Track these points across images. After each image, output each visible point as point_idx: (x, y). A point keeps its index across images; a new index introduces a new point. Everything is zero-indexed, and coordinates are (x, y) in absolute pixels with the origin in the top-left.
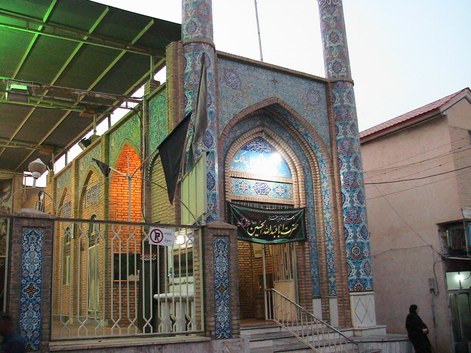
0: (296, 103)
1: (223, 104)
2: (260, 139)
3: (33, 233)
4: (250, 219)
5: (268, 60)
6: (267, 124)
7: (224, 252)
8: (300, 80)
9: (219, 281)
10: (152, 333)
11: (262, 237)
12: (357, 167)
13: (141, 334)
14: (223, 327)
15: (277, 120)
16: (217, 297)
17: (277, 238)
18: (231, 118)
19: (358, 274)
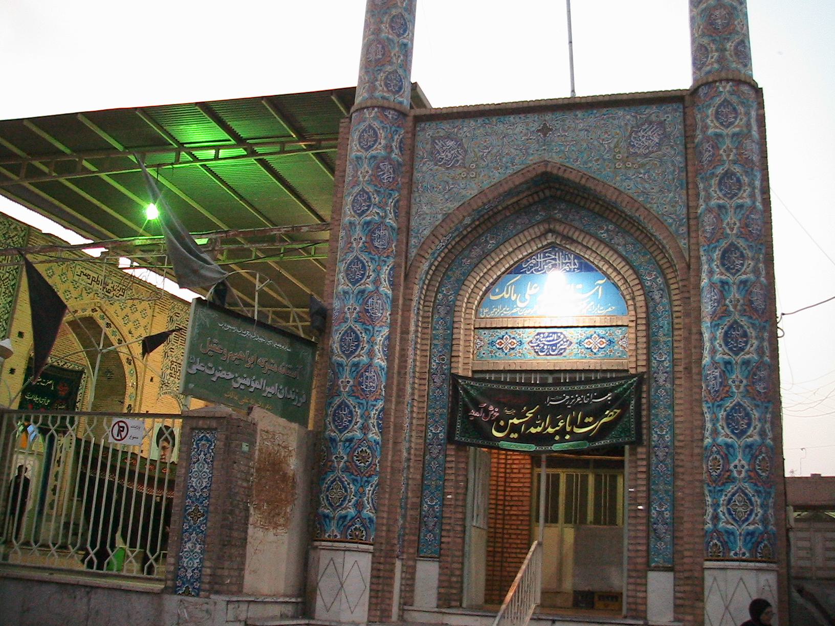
1: (424, 200)
2: (552, 246)
6: (559, 216)
7: (208, 455)
8: (613, 111)
9: (193, 502)
10: (94, 570)
12: (728, 269)
13: (141, 575)
14: (189, 575)
16: (186, 527)
17: (562, 440)
18: (437, 223)
19: (716, 518)
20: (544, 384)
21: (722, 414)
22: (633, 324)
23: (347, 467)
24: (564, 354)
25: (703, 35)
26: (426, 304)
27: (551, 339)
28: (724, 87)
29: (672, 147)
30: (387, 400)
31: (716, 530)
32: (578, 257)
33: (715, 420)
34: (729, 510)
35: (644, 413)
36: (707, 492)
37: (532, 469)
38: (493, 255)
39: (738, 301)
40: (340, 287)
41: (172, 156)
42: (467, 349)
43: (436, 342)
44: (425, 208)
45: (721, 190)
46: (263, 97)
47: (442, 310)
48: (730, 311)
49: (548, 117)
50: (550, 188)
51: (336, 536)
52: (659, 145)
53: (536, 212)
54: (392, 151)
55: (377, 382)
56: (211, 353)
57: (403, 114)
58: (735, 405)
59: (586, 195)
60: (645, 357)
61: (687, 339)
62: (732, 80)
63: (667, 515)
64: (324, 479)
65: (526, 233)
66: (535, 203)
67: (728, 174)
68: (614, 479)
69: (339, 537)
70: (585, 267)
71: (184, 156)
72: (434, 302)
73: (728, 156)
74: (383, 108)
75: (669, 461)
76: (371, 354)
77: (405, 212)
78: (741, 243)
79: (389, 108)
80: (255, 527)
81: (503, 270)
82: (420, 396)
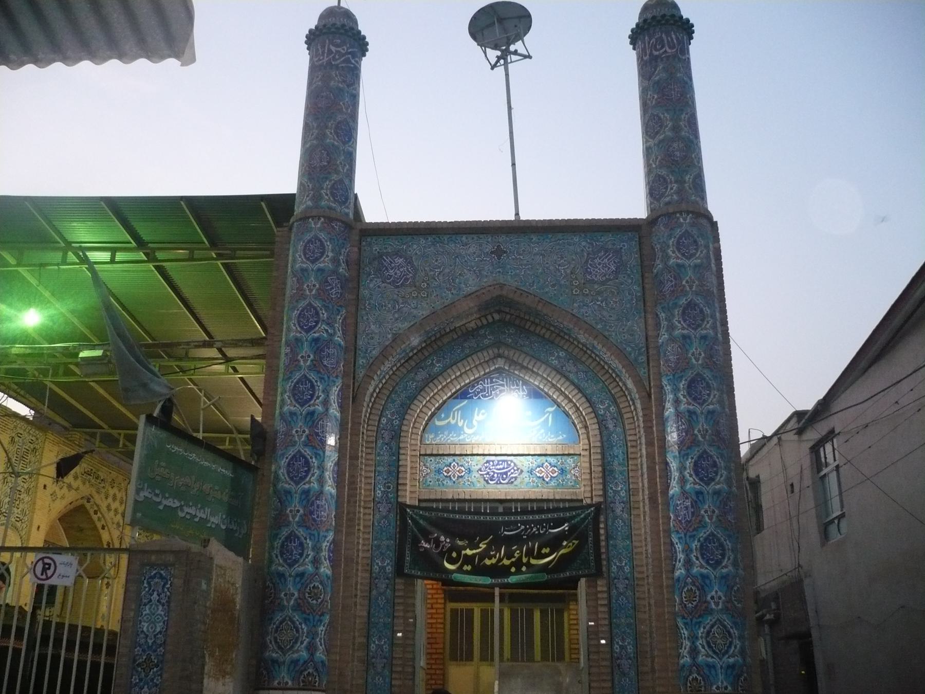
0: (553, 286)
2: (499, 371)
3: (158, 576)
4: (452, 534)
5: (529, 214)
7: (163, 595)
9: (144, 651)
11: (479, 570)
12: (695, 399)
15: (532, 329)
17: (519, 571)
18: (387, 343)
19: (694, 652)
20: (494, 512)
21: (695, 544)
22: (587, 453)
23: (299, 605)
24: (515, 483)
25: (661, 166)
26: (369, 428)
27: (501, 467)
28: (685, 219)
29: (629, 275)
30: (337, 531)
31: (695, 664)
32: (525, 383)
33: (687, 551)
34: (708, 643)
35: (603, 544)
36: (681, 625)
37: (445, 604)
38: (440, 378)
39: (707, 431)
40: (286, 409)
41: (58, 256)
42: (414, 476)
43: (380, 469)
44: (373, 327)
45: (685, 321)
46: (182, 198)
47: (387, 435)
48: (699, 441)
49: (502, 238)
50: (499, 312)
51: (287, 683)
52: (617, 272)
53: (485, 337)
54: (340, 265)
55: (327, 512)
56: (158, 478)
57: (348, 226)
58: (709, 535)
59: (537, 321)
60: (601, 487)
61: (651, 469)
62: (692, 212)
63: (630, 649)
64: (272, 619)
65: (474, 357)
66: (483, 327)
67: (691, 305)
68: (560, 612)
69: (290, 683)
70: (536, 394)
71: (71, 257)
72: (378, 426)
73: (691, 287)
74: (330, 220)
75: (629, 593)
76: (321, 481)
77: (352, 330)
78: (707, 374)
79: (337, 220)
80: (209, 677)
81: (449, 394)
82: (365, 527)
